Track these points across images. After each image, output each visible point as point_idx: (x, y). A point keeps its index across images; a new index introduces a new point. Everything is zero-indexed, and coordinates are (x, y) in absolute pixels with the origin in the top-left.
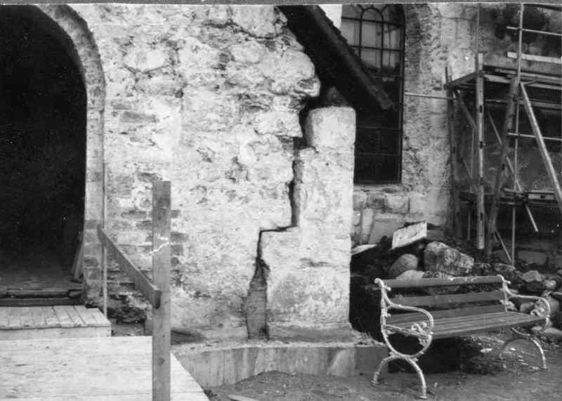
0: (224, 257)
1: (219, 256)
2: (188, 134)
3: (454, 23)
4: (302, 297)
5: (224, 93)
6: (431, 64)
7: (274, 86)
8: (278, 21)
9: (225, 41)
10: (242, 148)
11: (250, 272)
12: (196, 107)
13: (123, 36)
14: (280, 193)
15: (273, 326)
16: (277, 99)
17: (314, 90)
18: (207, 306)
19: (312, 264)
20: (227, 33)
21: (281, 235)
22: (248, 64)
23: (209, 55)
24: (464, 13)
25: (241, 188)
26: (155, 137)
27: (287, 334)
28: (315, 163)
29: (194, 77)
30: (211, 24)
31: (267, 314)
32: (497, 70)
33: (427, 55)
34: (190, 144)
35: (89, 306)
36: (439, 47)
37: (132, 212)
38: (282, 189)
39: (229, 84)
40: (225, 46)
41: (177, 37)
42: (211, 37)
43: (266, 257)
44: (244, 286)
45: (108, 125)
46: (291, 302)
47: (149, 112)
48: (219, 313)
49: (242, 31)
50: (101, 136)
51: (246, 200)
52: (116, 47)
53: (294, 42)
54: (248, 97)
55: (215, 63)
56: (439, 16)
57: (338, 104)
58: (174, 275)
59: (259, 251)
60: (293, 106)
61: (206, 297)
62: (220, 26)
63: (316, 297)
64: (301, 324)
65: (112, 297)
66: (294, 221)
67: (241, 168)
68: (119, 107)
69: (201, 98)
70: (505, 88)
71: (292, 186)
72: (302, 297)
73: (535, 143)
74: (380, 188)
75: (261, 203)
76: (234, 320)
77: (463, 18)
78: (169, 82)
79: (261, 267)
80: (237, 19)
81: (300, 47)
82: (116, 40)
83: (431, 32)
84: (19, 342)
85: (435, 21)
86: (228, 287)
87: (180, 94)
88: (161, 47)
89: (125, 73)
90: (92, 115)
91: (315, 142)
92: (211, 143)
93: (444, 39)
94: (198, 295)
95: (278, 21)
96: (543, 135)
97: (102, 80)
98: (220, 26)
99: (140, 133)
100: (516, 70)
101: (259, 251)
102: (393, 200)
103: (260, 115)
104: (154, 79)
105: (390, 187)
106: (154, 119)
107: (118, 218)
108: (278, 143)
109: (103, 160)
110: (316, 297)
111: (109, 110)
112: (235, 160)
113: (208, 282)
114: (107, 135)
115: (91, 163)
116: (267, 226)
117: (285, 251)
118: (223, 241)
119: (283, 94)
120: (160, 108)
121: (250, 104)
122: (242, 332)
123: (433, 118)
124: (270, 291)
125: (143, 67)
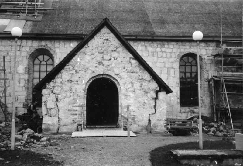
0: (143, 119)
1: (142, 119)
2: (136, 98)
3: (210, 64)
4: (157, 126)
5: (142, 91)
6: (204, 75)
7: (151, 89)
8: (151, 78)
9: (141, 82)
10: (145, 100)
11: (148, 122)
12: (137, 93)
13: (124, 83)
14: (152, 107)
15: (152, 131)
16: (151, 91)
18: (140, 128)
19: (159, 120)
20: (142, 80)
21: (153, 115)
22: (146, 85)
23: (139, 84)
24: (212, 61)
25: (145, 107)
26: (130, 99)
27: (154, 132)
28: (159, 102)
29: (136, 88)
30: (139, 79)
31: (151, 129)
32: (218, 77)
33: (203, 73)
34: (136, 100)
35: (122, 104)
36: (206, 71)
38: (153, 107)
39: (142, 89)
40: (141, 83)
41: (133, 82)
42: (139, 81)
43: (151, 119)
44: (147, 124)
45: (122, 97)
46: (155, 127)
48: (142, 129)
49: (144, 80)
50: (121, 99)
51: (146, 109)
52: (123, 85)
53: (154, 81)
54: (146, 91)
55: (140, 86)
56: (205, 63)
57: (163, 91)
58: (134, 122)
59: (149, 118)
60: (154, 92)
61: (140, 126)
62: (141, 79)
63: (160, 126)
64: (157, 131)
65: (124, 126)
66: (155, 112)
67: (145, 103)
68: (124, 94)
70: (220, 81)
71: (155, 106)
72: (157, 126)
73: (225, 93)
74: (193, 108)
75: (149, 109)
76: (145, 130)
77: (212, 63)
78: (133, 89)
79: (149, 121)
81: (155, 82)
82: (123, 83)
83: (203, 67)
85: (204, 64)
86: (144, 124)
87: (134, 91)
88: (131, 84)
89: (125, 88)
90: (119, 96)
91: (159, 98)
92: (140, 99)
93: (207, 68)
94: (138, 126)
95: (151, 78)
96: (227, 92)
97: (121, 90)
98: (141, 79)
99: (128, 98)
100: (222, 76)
101: (149, 118)
102: (196, 110)
103: (148, 94)
104: (130, 89)
105: (196, 107)
106: (130, 96)
107: (125, 113)
108: (152, 99)
109: (168, 23)
110: (160, 126)
111: (122, 95)
112: (144, 102)
113: (140, 123)
114: (122, 99)
115: (120, 104)
116: (150, 113)
117: (154, 118)
118: (143, 116)
119: (152, 90)
120: (132, 94)
121: (146, 92)
122: (147, 132)
123: (205, 89)
124: (151, 125)
125: (128, 87)
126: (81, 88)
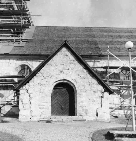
17: (103, 90)
19: (104, 113)
25: (94, 103)
37: (81, 106)
41: (85, 85)
43: (98, 112)
47: (82, 94)
59: (97, 111)
69: (88, 92)
80: (93, 82)
84: (88, 75)
87: (86, 92)
101: (97, 111)
108: (98, 97)
112: (93, 100)
119: (99, 91)
121: (95, 92)
126: (49, 89)
